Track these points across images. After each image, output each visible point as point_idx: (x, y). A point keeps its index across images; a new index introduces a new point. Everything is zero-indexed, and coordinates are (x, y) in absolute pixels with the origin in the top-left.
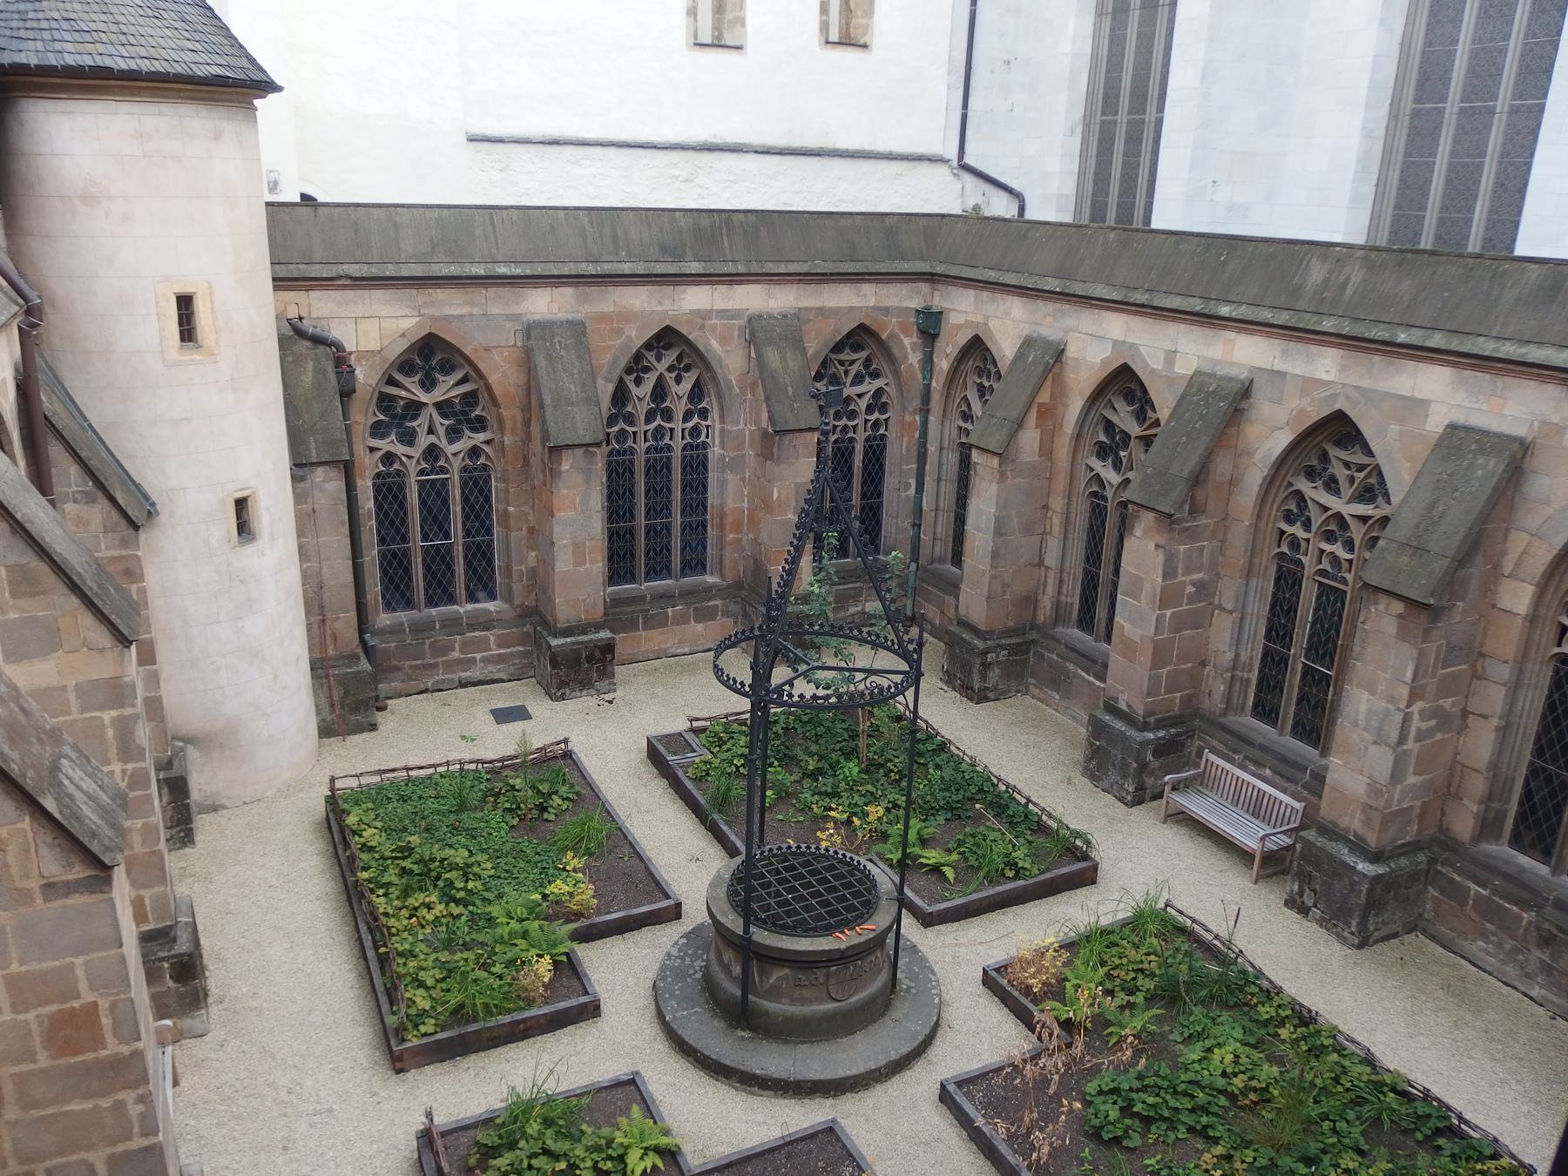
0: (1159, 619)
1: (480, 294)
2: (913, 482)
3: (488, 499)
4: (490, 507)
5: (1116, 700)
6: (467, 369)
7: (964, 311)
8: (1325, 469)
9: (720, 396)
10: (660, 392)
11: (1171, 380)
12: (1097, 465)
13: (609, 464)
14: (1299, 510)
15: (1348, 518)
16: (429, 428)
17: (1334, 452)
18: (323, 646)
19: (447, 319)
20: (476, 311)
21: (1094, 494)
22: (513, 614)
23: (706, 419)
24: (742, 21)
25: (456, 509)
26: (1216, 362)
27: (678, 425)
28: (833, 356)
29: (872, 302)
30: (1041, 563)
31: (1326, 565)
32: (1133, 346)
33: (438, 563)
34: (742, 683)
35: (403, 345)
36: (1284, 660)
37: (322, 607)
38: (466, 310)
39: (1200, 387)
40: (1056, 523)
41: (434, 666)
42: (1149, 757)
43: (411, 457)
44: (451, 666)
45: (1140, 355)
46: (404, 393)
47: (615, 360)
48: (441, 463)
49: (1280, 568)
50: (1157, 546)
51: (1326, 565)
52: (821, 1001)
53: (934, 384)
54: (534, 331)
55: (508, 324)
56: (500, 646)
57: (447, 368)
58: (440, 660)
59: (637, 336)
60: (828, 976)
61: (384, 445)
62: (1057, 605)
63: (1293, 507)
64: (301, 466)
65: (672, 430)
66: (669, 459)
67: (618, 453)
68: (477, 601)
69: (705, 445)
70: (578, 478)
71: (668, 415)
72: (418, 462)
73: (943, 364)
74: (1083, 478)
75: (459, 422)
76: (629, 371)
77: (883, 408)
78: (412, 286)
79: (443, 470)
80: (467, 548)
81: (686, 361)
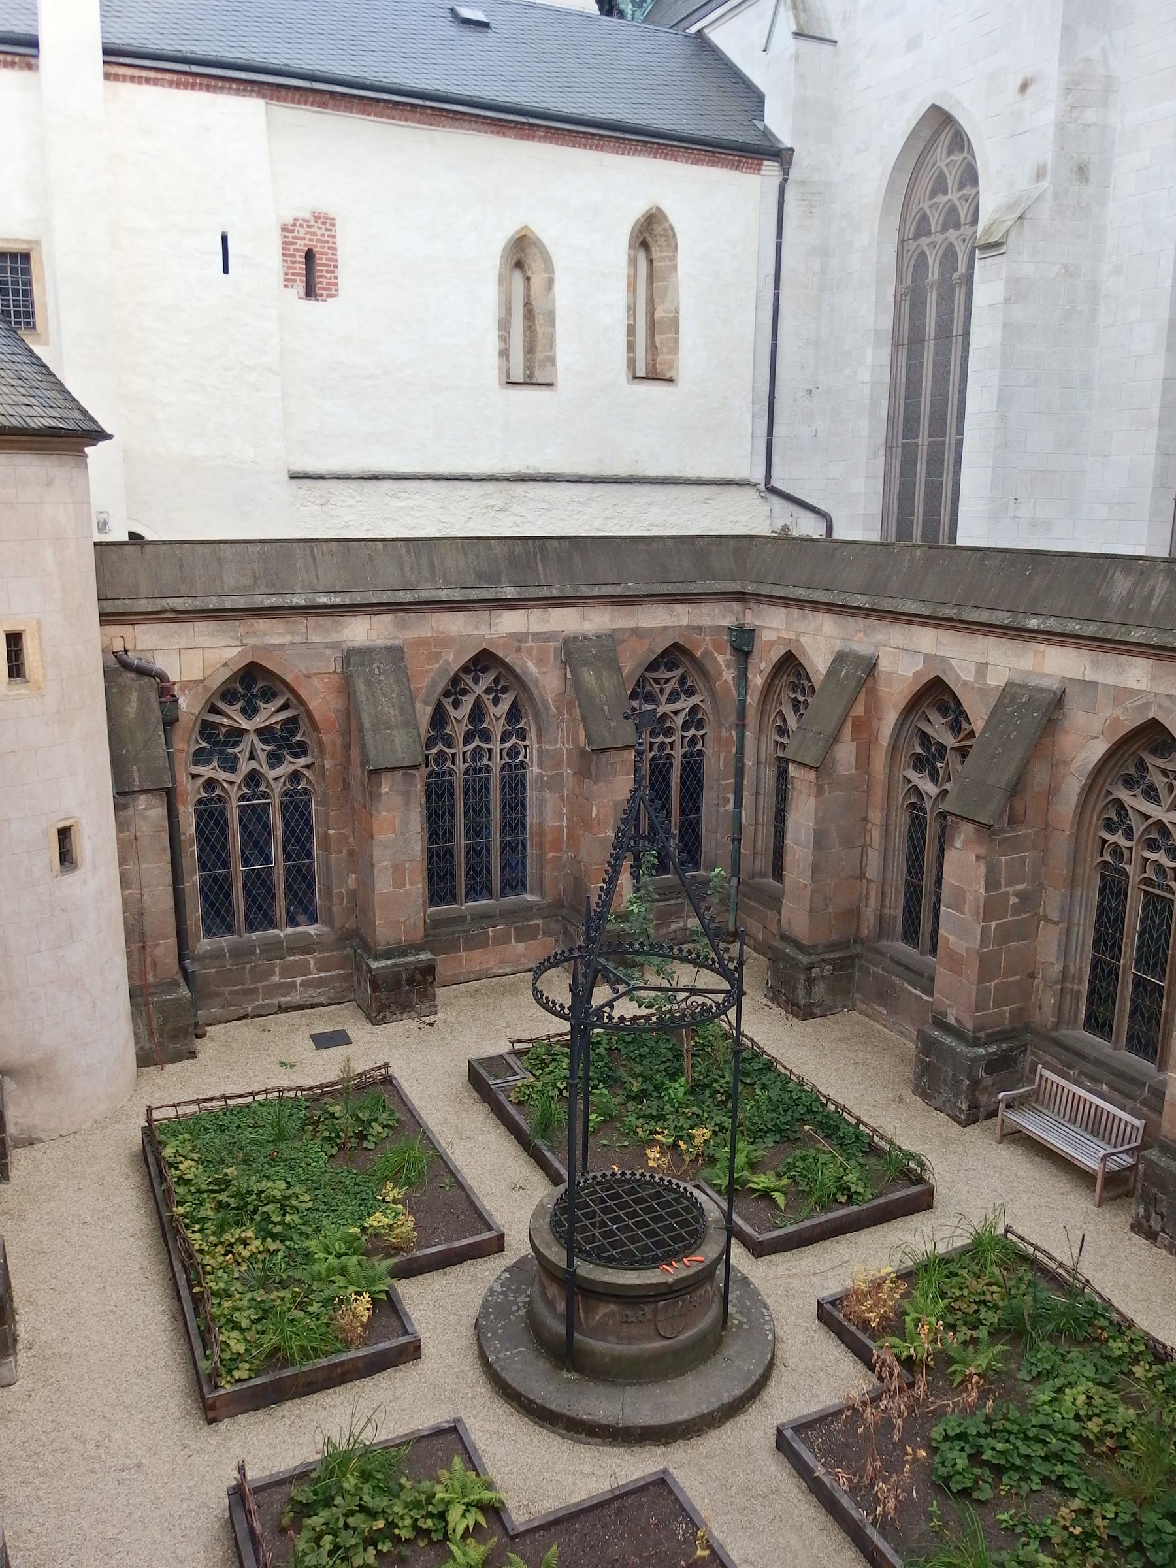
0: (985, 931)
1: (301, 624)
2: (731, 797)
3: (308, 823)
4: (311, 830)
5: (945, 1015)
6: (288, 695)
7: (775, 627)
8: (1143, 777)
9: (537, 715)
10: (478, 713)
11: (983, 692)
12: (914, 776)
13: (429, 785)
14: (1119, 819)
15: (1169, 825)
16: (251, 755)
17: (1151, 760)
18: (143, 974)
19: (268, 648)
20: (297, 639)
21: (913, 806)
22: (333, 937)
23: (524, 739)
24: (552, 360)
25: (277, 832)
26: (1027, 673)
27: (496, 746)
28: (648, 675)
29: (685, 621)
30: (862, 876)
31: (1150, 874)
32: (944, 659)
33: (259, 885)
34: (561, 1006)
35: (226, 674)
36: (1114, 972)
37: (142, 934)
38: (287, 639)
39: (1013, 698)
40: (876, 834)
41: (255, 991)
42: (982, 1073)
43: (232, 783)
44: (271, 990)
45: (952, 668)
46: (226, 721)
47: (434, 683)
48: (262, 788)
49: (1103, 878)
50: (978, 857)
51: (1150, 874)
52: (650, 1339)
53: (749, 699)
54: (353, 657)
55: (328, 652)
56: (320, 970)
57: (269, 695)
58: (260, 984)
59: (454, 660)
60: (655, 1312)
61: (206, 772)
62: (881, 919)
63: (1113, 815)
64: (123, 795)
65: (490, 750)
66: (488, 779)
67: (437, 774)
68: (298, 925)
69: (523, 765)
70: (398, 800)
71: (486, 736)
72: (239, 788)
73: (757, 681)
74: (901, 790)
75: (280, 748)
76: (447, 694)
77: (700, 725)
78: (235, 618)
79: (264, 795)
80: (288, 871)
81: (503, 683)
